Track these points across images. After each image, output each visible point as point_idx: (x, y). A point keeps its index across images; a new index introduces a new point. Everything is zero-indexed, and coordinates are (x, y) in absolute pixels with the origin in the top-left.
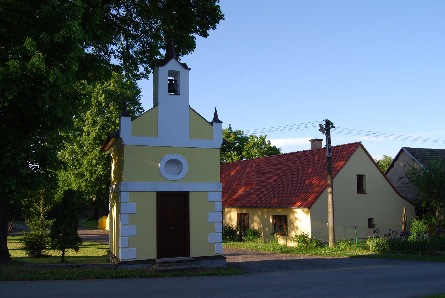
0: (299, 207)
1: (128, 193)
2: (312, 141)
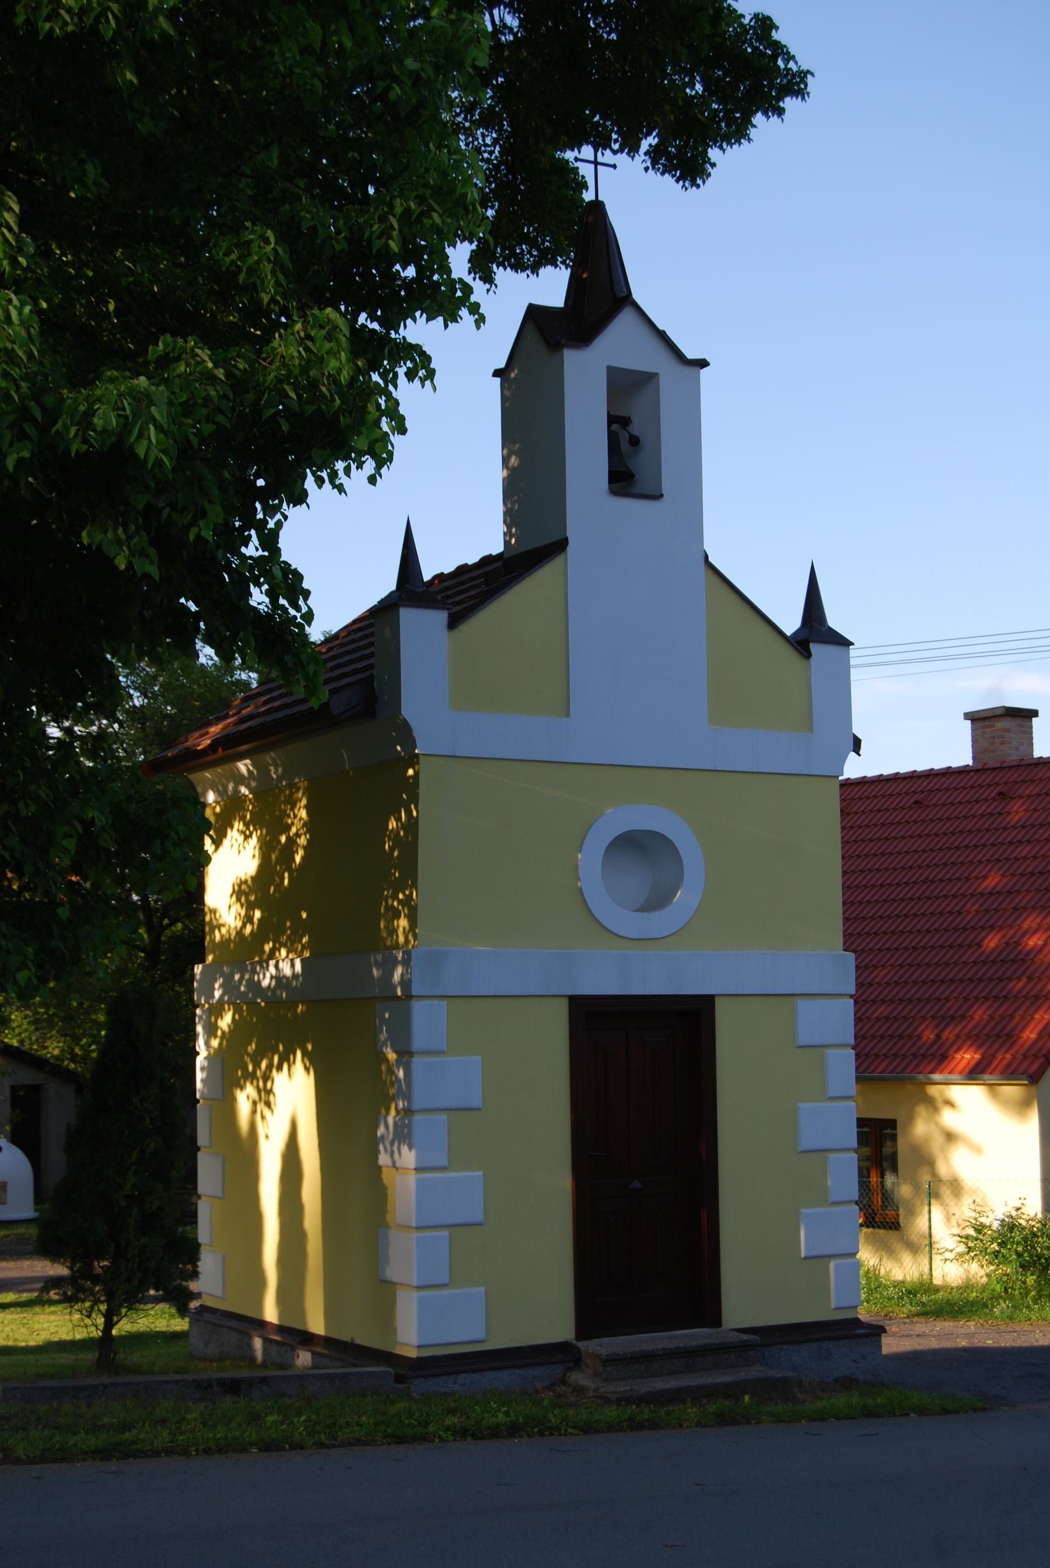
0: (973, 1074)
1: (444, 1003)
2: (977, 719)
